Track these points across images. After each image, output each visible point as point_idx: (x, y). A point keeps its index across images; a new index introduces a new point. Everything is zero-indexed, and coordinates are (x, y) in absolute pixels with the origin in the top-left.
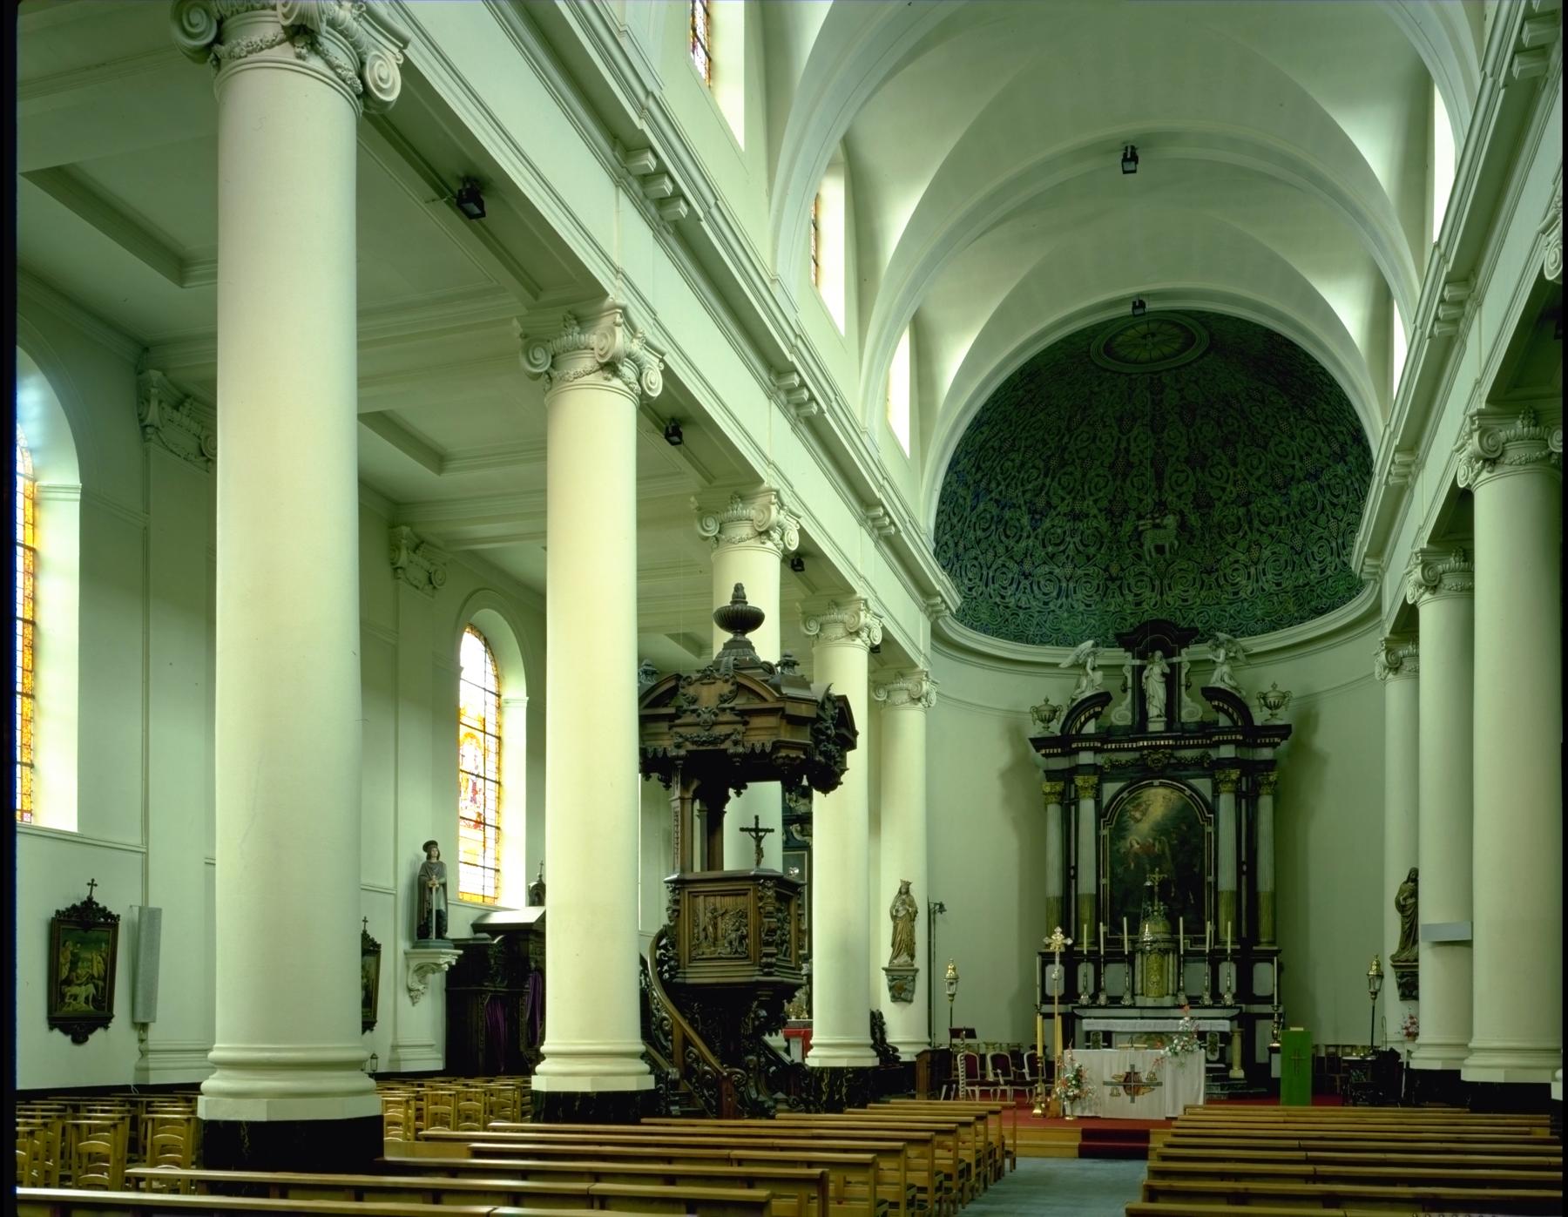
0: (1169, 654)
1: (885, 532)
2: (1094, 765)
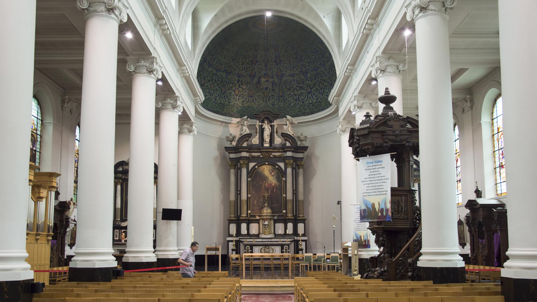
0: (270, 121)
1: (185, 75)
2: (292, 157)
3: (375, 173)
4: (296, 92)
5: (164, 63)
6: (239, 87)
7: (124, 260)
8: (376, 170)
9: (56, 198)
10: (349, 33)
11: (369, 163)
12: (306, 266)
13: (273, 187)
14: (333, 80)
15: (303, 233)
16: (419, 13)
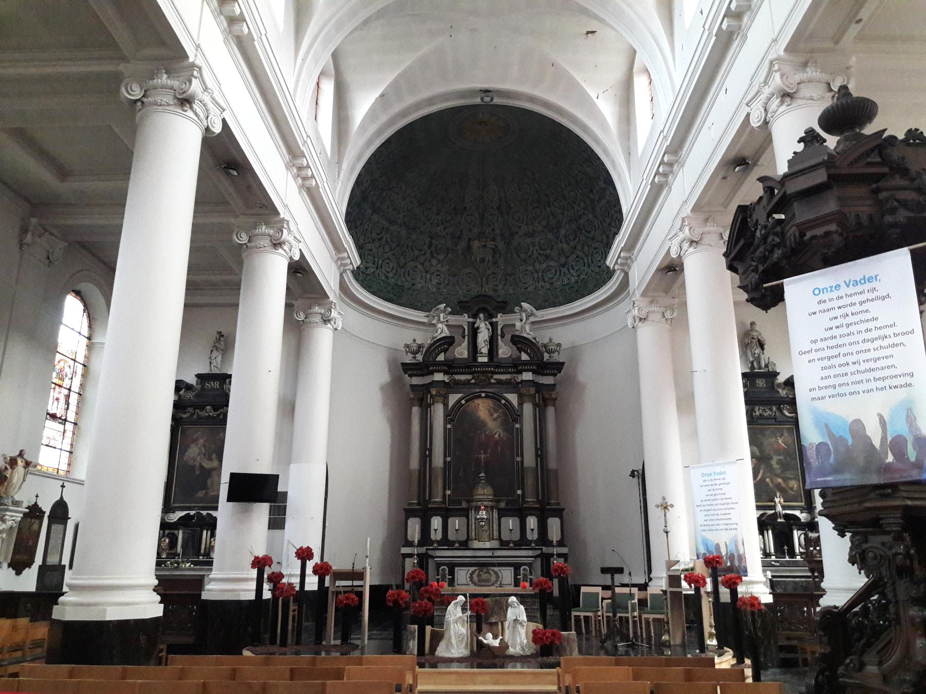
0: (490, 316)
3: (850, 319)
4: (537, 266)
6: (433, 257)
13: (497, 442)
14: (611, 236)
15: (559, 538)
16: (779, 107)
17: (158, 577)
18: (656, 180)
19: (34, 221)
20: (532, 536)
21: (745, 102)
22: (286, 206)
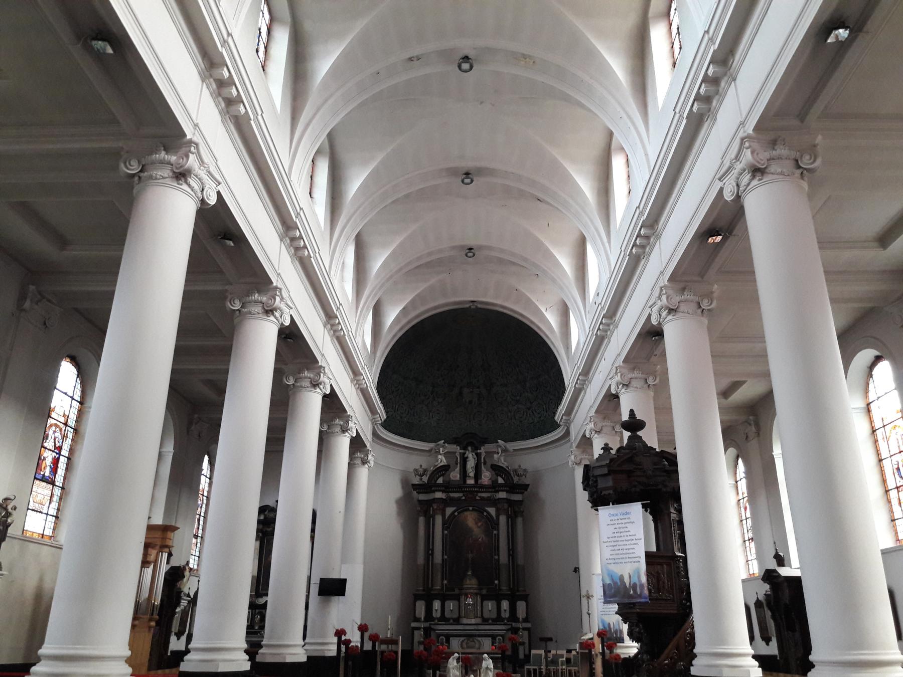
0: (476, 448)
1: (338, 334)
5: (335, 374)
7: (258, 659)
8: (624, 525)
9: (168, 562)
10: (577, 335)
11: (612, 515)
12: (535, 670)
15: (524, 615)
16: (751, 180)
17: (247, 642)
18: (695, 108)
19: (32, 288)
20: (506, 615)
21: (718, 176)
22: (279, 274)
